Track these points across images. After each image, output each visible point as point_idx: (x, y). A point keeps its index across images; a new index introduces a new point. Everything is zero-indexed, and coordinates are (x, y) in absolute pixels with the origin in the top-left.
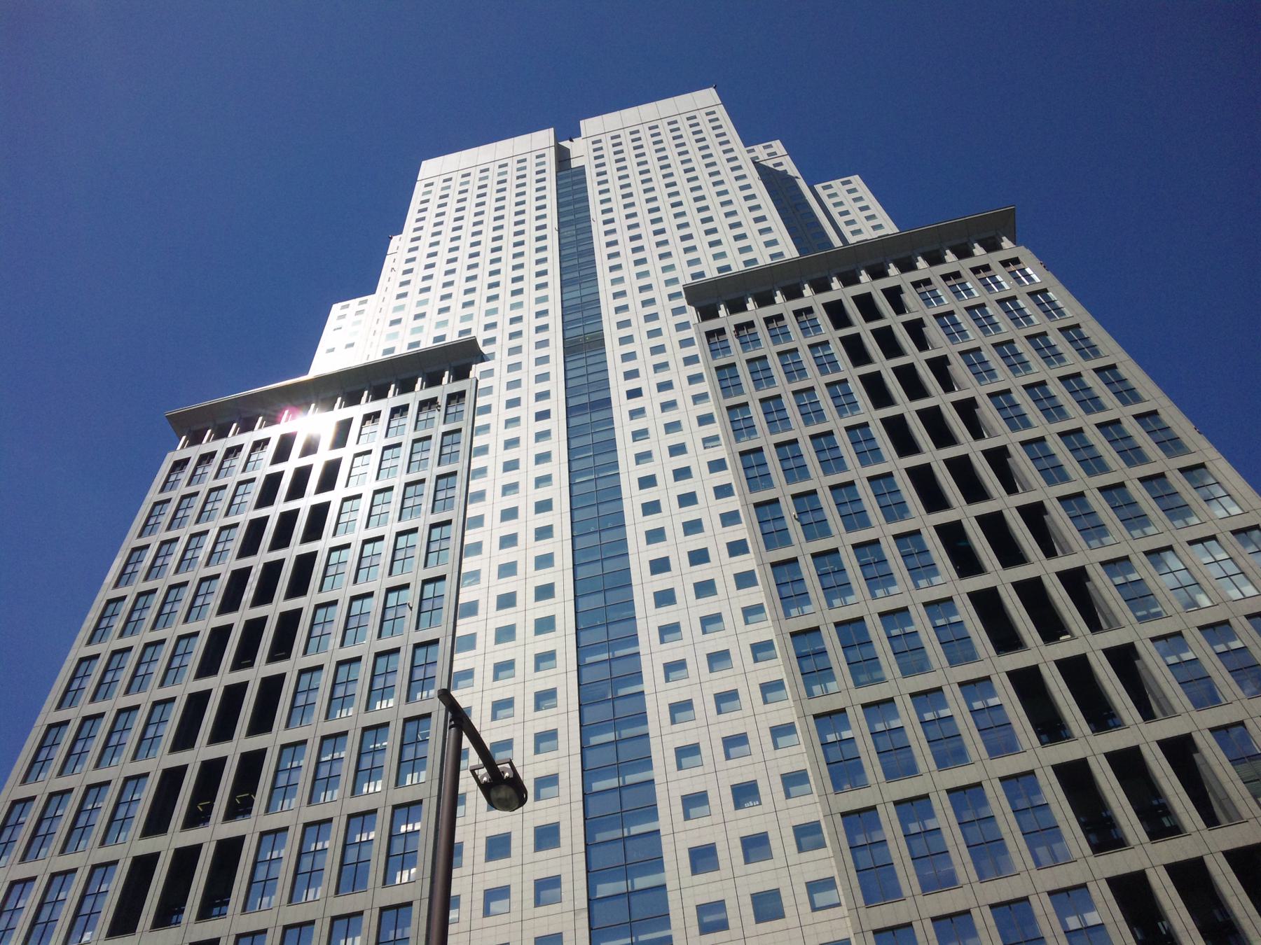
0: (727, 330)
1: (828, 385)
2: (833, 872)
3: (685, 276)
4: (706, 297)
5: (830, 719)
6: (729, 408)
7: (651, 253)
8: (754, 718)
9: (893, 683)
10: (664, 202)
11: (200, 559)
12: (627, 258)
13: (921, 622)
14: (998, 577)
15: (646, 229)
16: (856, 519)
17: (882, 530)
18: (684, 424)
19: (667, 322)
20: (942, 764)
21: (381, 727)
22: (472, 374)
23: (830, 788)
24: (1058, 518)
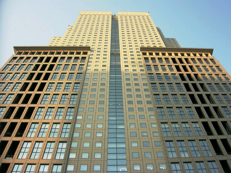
3: (140, 45)
19: (135, 54)
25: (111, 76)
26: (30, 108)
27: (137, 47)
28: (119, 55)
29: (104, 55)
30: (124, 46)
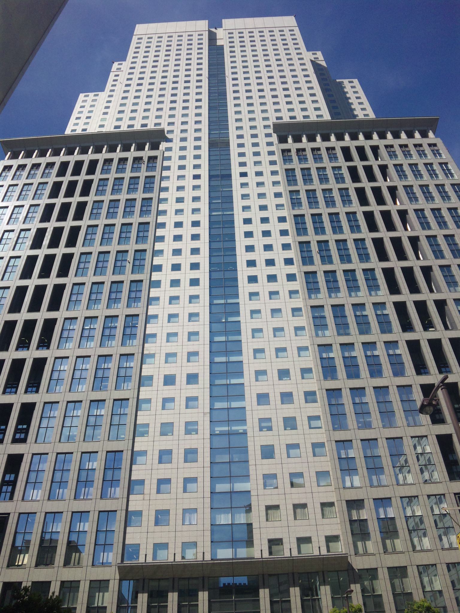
0: (292, 150)
1: (339, 189)
2: (320, 414)
4: (284, 131)
5: (333, 393)
6: (290, 191)
7: (256, 101)
8: (291, 342)
9: (354, 336)
10: (264, 75)
11: (20, 219)
12: (243, 101)
13: (369, 311)
14: (407, 297)
15: (254, 88)
16: (345, 258)
17: (357, 265)
18: (268, 195)
19: (262, 140)
20: (372, 375)
21: (107, 357)
22: (161, 148)
23: (322, 378)
24: (437, 274)
25: (213, 214)
26: (79, 203)
27: (266, 123)
28: (227, 144)
29: (198, 81)
30: (230, 47)
